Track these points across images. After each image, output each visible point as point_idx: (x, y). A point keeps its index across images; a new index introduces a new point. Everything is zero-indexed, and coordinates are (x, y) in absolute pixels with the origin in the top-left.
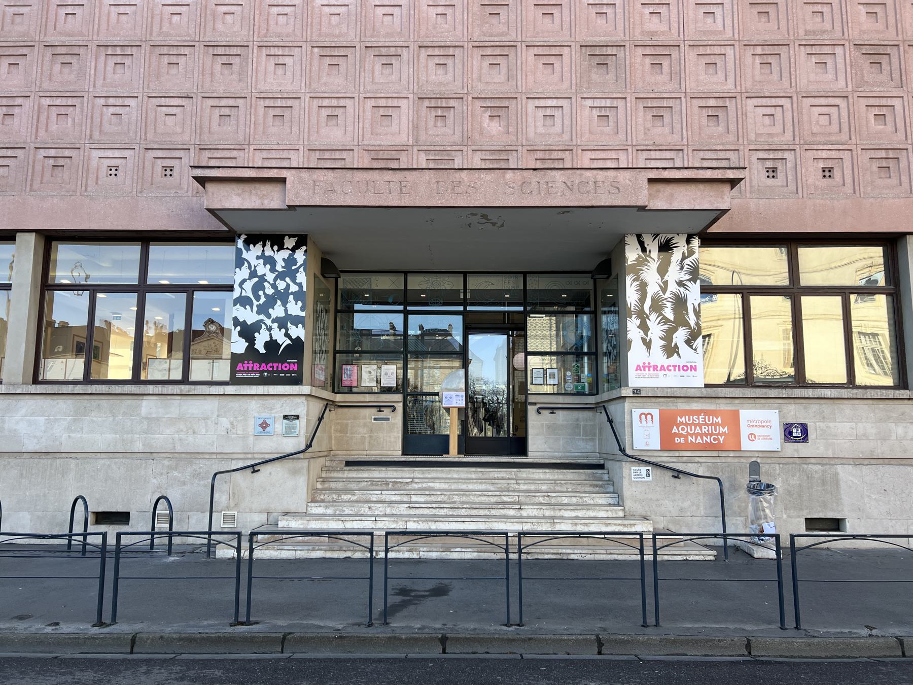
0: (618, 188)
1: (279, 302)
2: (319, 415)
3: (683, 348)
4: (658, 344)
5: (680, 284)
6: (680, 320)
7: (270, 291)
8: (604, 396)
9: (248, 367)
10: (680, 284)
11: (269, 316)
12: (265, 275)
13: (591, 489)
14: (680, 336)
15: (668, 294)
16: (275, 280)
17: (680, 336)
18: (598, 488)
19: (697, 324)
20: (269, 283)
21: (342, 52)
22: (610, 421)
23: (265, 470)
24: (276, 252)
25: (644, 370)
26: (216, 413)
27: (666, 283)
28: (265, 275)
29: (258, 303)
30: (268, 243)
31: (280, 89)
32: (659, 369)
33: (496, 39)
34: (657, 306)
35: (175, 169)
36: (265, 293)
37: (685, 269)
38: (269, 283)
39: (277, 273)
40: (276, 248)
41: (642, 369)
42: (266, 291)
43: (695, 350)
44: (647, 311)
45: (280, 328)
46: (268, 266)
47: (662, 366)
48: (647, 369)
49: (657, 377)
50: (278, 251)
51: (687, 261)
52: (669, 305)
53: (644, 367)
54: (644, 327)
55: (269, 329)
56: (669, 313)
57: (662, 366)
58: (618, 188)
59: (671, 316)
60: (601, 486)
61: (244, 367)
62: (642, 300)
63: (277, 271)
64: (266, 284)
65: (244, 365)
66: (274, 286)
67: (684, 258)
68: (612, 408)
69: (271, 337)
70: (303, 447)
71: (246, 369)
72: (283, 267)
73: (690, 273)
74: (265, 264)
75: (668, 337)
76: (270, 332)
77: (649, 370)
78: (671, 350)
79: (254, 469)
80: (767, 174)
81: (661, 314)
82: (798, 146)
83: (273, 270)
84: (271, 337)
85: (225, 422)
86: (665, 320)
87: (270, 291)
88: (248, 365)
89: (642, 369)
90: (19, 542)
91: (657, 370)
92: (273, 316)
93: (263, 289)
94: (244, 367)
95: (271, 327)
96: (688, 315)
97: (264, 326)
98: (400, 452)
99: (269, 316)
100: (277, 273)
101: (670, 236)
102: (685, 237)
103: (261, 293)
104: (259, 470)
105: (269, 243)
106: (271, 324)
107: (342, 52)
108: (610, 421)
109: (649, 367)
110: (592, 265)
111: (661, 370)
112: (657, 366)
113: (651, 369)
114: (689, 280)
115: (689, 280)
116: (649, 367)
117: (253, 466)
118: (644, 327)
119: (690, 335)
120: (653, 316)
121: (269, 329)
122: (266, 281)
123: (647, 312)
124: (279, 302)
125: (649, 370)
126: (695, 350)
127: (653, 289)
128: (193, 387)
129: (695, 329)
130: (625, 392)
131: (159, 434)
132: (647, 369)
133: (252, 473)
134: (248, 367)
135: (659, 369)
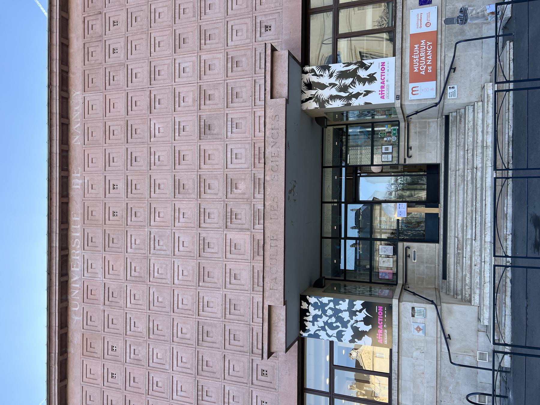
0: (276, 116)
2: (411, 295)
3: (370, 71)
4: (368, 87)
5: (331, 76)
6: (353, 74)
8: (400, 117)
10: (331, 76)
11: (348, 321)
13: (463, 123)
14: (363, 73)
15: (337, 83)
16: (326, 316)
17: (363, 73)
18: (462, 119)
19: (355, 64)
20: (328, 319)
21: (202, 270)
22: (417, 112)
23: (448, 331)
24: (310, 314)
26: (411, 358)
27: (330, 84)
28: (324, 322)
29: (341, 327)
31: (220, 305)
33: (196, 186)
34: (344, 89)
35: (263, 369)
36: (335, 323)
37: (322, 74)
38: (328, 319)
40: (308, 314)
43: (371, 64)
45: (356, 315)
46: (319, 319)
50: (309, 313)
51: (318, 73)
52: (343, 82)
54: (357, 95)
55: (357, 321)
56: (349, 81)
58: (276, 116)
59: (351, 80)
60: (461, 117)
62: (340, 97)
66: (330, 317)
67: (315, 75)
68: (408, 112)
69: (362, 321)
70: (433, 306)
74: (317, 321)
75: (363, 81)
78: (372, 78)
79: (448, 338)
82: (254, 15)
83: (321, 317)
84: (362, 321)
85: (416, 354)
86: (353, 83)
87: (333, 319)
92: (349, 318)
93: (332, 323)
95: (355, 321)
96: (349, 70)
97: (355, 325)
98: (437, 244)
99: (348, 321)
103: (334, 325)
104: (449, 335)
105: (305, 317)
106: (354, 320)
107: (202, 270)
108: (417, 112)
109: (382, 91)
110: (318, 128)
114: (329, 71)
115: (329, 71)
116: (382, 91)
117: (446, 338)
118: (357, 95)
119: (362, 68)
120: (350, 90)
121: (357, 321)
122: (327, 321)
124: (340, 315)
126: (371, 64)
127: (334, 92)
128: (393, 371)
129: (358, 65)
130: (398, 104)
131: (424, 396)
133: (450, 339)
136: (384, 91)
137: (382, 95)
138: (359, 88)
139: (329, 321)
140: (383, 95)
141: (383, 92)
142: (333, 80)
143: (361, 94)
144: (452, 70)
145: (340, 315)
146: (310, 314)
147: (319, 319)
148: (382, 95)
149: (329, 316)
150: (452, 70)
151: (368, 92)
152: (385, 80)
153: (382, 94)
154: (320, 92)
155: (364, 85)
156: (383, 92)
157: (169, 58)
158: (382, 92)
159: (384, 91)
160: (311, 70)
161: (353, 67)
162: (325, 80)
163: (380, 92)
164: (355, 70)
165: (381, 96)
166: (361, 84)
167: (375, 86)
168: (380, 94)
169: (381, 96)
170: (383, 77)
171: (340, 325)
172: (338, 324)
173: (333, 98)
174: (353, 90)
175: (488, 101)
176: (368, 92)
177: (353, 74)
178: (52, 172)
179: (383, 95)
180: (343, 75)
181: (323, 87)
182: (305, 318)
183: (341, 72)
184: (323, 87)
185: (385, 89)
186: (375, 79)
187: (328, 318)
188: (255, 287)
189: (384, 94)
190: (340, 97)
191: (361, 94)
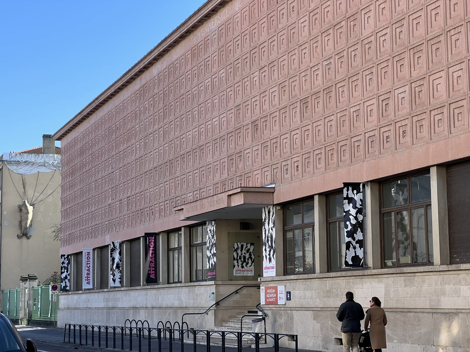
3: (245, 266)
4: (240, 266)
5: (245, 253)
6: (245, 261)
9: (153, 270)
10: (245, 253)
11: (354, 239)
12: (349, 210)
14: (244, 264)
15: (242, 256)
16: (357, 214)
17: (244, 264)
20: (353, 216)
24: (355, 195)
27: (242, 253)
28: (349, 210)
29: (347, 230)
30: (350, 188)
32: (89, 272)
34: (240, 258)
36: (350, 223)
38: (353, 216)
39: (357, 209)
40: (355, 192)
42: (351, 221)
44: (238, 259)
45: (361, 247)
46: (351, 205)
47: (87, 270)
49: (241, 273)
50: (357, 194)
51: (246, 249)
52: (242, 258)
53: (238, 270)
54: (238, 262)
55: (355, 248)
56: (242, 260)
57: (87, 270)
59: (243, 260)
61: (153, 273)
62: (237, 257)
63: (357, 208)
64: (351, 217)
65: (151, 273)
66: (356, 218)
67: (246, 248)
69: (355, 254)
71: (154, 272)
72: (360, 205)
74: (349, 203)
75: (242, 264)
76: (355, 250)
78: (242, 267)
81: (119, 269)
83: (355, 207)
84: (355, 254)
86: (242, 261)
88: (151, 270)
91: (90, 273)
92: (356, 239)
93: (349, 220)
94: (153, 273)
95: (355, 246)
97: (351, 246)
99: (354, 239)
100: (357, 209)
101: (243, 243)
102: (246, 243)
105: (351, 188)
106: (355, 245)
109: (239, 270)
111: (89, 271)
112: (88, 273)
116: (239, 270)
118: (238, 262)
120: (239, 260)
121: (355, 248)
122: (351, 215)
123: (115, 269)
124: (359, 230)
127: (239, 254)
134: (153, 270)
135: (89, 272)
136: (89, 277)
137: (87, 281)
138: (240, 263)
139: (351, 217)
140: (89, 281)
141: (89, 279)
142: (243, 254)
143: (114, 277)
144: (236, 292)
145: (359, 230)
146: (355, 195)
147: (351, 205)
148: (87, 281)
149: (356, 216)
150: (236, 292)
151: (238, 266)
152: (244, 272)
153: (88, 280)
154: (240, 250)
155: (119, 278)
156: (89, 279)
157: (298, 155)
158: (87, 279)
159: (89, 277)
161: (247, 261)
163: (86, 279)
164: (246, 262)
165: (87, 281)
166: (119, 277)
168: (86, 280)
169: (87, 281)
170: (245, 271)
171: (349, 229)
172: (350, 228)
173: (238, 254)
174: (239, 261)
175: (88, 274)
176: (238, 266)
179: (89, 281)
181: (241, 251)
185: (240, 272)
186: (242, 268)
187: (355, 215)
188: (319, 155)
189: (89, 280)
190: (237, 257)
191: (114, 277)
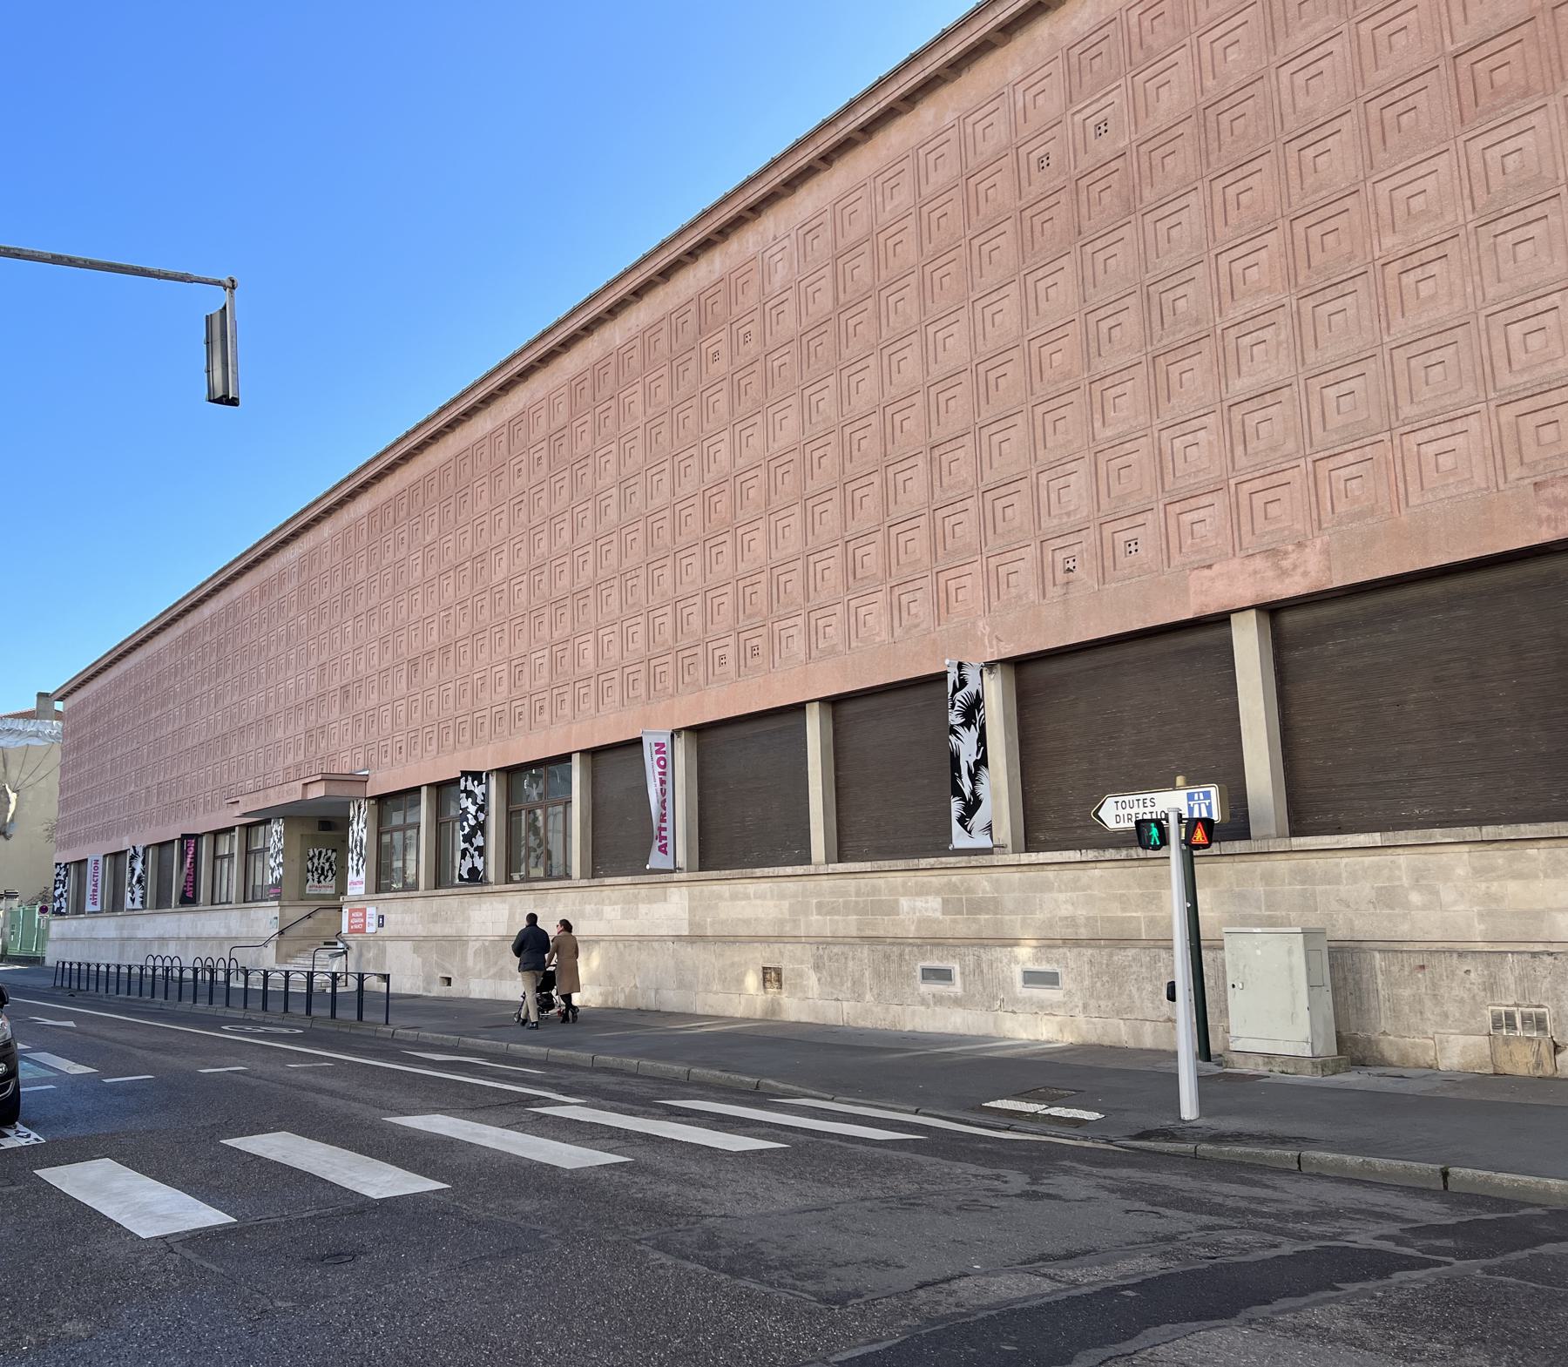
1: (479, 833)
6: (323, 873)
7: (472, 822)
11: (472, 845)
16: (477, 812)
19: (973, 793)
25: (665, 838)
34: (317, 870)
36: (469, 825)
37: (956, 708)
40: (476, 783)
41: (664, 842)
43: (970, 832)
45: (480, 856)
48: (663, 834)
51: (958, 696)
55: (472, 857)
66: (476, 817)
73: (964, 715)
77: (665, 829)
78: (319, 882)
80: (1134, 552)
83: (475, 803)
87: (472, 822)
89: (664, 842)
90: (932, 860)
93: (467, 820)
96: (960, 777)
99: (472, 845)
103: (465, 824)
113: (663, 825)
114: (962, 725)
115: (962, 725)
119: (964, 809)
121: (472, 857)
124: (479, 833)
125: (665, 829)
126: (970, 832)
129: (970, 800)
132: (663, 834)
138: (316, 876)
139: (469, 816)
160: (963, 679)
162: (322, 860)
167: (316, 883)
171: (466, 832)
177: (323, 873)
178: (632, 274)
180: (323, 868)
181: (319, 859)
182: (470, 779)
183: (958, 757)
184: (319, 859)
